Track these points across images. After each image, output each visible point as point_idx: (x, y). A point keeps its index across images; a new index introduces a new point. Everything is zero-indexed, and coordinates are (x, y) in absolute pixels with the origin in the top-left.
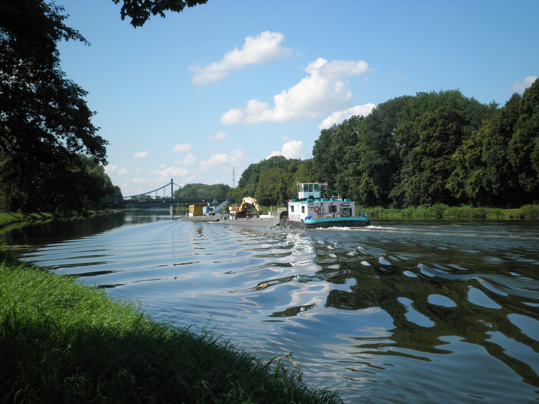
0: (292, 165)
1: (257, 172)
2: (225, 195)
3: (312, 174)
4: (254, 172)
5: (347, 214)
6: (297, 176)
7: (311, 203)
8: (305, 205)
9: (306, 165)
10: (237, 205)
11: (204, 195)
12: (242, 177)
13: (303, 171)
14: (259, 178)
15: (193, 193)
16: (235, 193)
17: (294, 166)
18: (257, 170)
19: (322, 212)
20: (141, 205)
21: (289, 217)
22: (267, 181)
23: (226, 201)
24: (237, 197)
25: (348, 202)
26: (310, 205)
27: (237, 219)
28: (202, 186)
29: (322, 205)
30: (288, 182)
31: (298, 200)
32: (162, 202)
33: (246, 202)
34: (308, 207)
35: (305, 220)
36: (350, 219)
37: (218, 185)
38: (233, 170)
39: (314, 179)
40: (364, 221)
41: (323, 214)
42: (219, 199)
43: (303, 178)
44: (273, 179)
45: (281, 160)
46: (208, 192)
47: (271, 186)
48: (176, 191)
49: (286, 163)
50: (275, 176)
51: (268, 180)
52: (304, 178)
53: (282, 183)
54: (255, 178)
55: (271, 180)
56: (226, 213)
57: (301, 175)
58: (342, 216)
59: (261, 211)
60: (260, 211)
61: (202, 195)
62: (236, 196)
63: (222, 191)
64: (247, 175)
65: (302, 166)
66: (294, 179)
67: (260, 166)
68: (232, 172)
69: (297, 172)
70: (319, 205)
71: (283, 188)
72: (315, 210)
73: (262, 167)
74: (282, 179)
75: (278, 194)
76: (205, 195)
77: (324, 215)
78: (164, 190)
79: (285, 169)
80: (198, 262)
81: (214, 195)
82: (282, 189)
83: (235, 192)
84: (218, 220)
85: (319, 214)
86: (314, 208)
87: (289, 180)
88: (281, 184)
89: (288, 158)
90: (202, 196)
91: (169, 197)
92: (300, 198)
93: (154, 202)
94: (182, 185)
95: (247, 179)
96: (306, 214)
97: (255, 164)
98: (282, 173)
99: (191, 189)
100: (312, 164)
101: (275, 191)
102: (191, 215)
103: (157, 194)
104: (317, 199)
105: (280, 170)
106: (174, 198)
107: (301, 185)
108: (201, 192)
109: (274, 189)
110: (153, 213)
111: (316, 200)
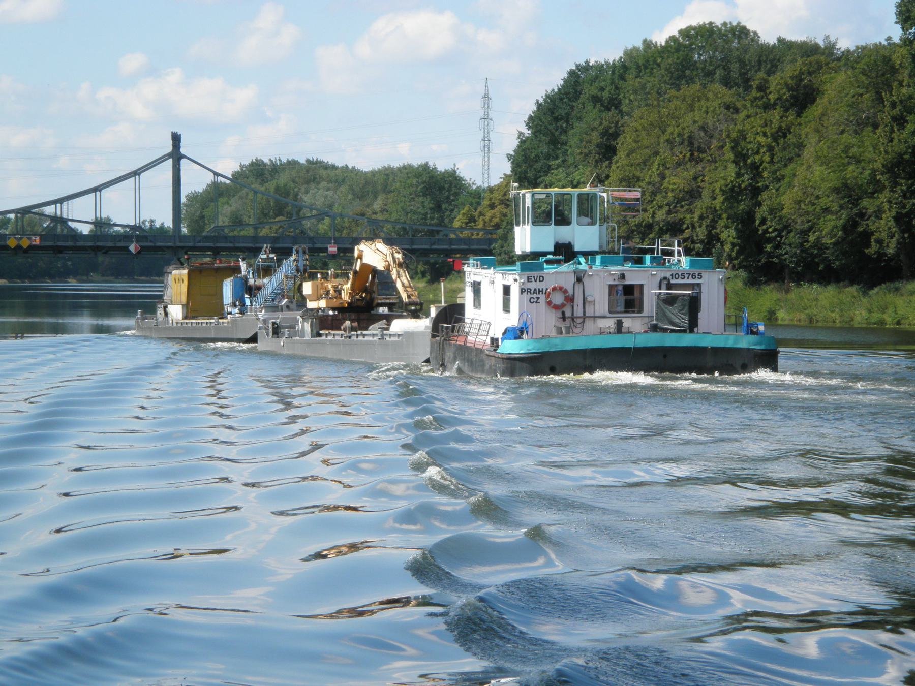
0: (788, 71)
1: (608, 109)
2: (441, 223)
3: (894, 119)
4: (589, 106)
5: (676, 320)
6: (817, 131)
7: (536, 274)
8: (509, 280)
9: (864, 73)
10: (336, 276)
11: (333, 218)
12: (527, 132)
13: (851, 106)
14: (616, 135)
15: (280, 210)
16: (489, 215)
17: (799, 78)
18: (606, 94)
19: (579, 312)
20: (20, 259)
21: (466, 330)
22: (656, 153)
23: (294, 257)
24: (500, 232)
25: (697, 271)
26: (529, 280)
27: (320, 335)
28: (324, 173)
29: (579, 280)
30: (767, 158)
31: (507, 259)
32: (126, 249)
33: (366, 260)
34: (522, 291)
35: (503, 339)
36: (687, 340)
37: (407, 170)
38: (486, 96)
39: (903, 147)
40: (748, 349)
41: (584, 317)
42: (412, 243)
43: (847, 138)
44: (691, 144)
45: (735, 44)
46: (358, 206)
47: (678, 180)
48: (193, 198)
49: (760, 63)
50: (703, 128)
51: (665, 152)
52: (854, 141)
53: (736, 163)
54: (596, 137)
55: (677, 150)
56: (293, 306)
57: (837, 123)
58: (654, 328)
59: (415, 304)
60: (411, 304)
61: (327, 220)
62: (497, 226)
63: (428, 203)
64: (556, 119)
65: (841, 77)
66: (801, 146)
67: (622, 78)
68: (478, 104)
69: (815, 111)
70: (568, 283)
71: (741, 191)
72: (549, 303)
73: (632, 81)
74: (736, 143)
75: (714, 221)
76: (338, 220)
77: (589, 324)
78: (137, 190)
79: (755, 93)
80: (354, 547)
81: (387, 221)
82: (733, 194)
83: (492, 206)
84: (254, 339)
85: (564, 318)
86: (548, 295)
87: (770, 149)
88: (732, 169)
89: (768, 37)
90: (324, 226)
91: (158, 225)
92: (518, 251)
93: (83, 248)
94: (228, 167)
95: (554, 142)
96: (513, 320)
97: (599, 68)
98: (737, 111)
99: (271, 186)
100: (894, 70)
101: (699, 203)
102: (176, 312)
103: (98, 206)
104: (586, 254)
105: (728, 95)
106: (185, 230)
107: (524, 195)
108: (319, 202)
109: (693, 194)
110: (76, 305)
111: (582, 260)
